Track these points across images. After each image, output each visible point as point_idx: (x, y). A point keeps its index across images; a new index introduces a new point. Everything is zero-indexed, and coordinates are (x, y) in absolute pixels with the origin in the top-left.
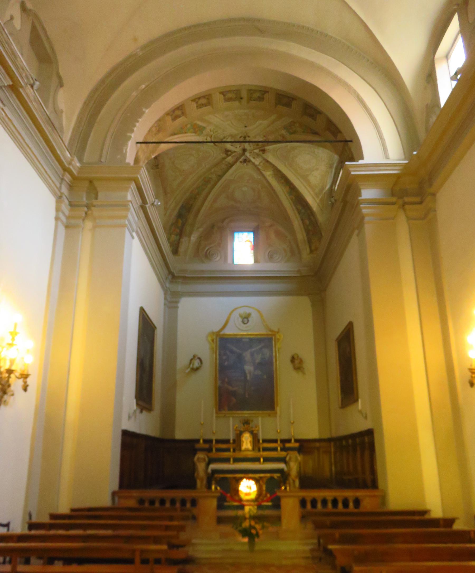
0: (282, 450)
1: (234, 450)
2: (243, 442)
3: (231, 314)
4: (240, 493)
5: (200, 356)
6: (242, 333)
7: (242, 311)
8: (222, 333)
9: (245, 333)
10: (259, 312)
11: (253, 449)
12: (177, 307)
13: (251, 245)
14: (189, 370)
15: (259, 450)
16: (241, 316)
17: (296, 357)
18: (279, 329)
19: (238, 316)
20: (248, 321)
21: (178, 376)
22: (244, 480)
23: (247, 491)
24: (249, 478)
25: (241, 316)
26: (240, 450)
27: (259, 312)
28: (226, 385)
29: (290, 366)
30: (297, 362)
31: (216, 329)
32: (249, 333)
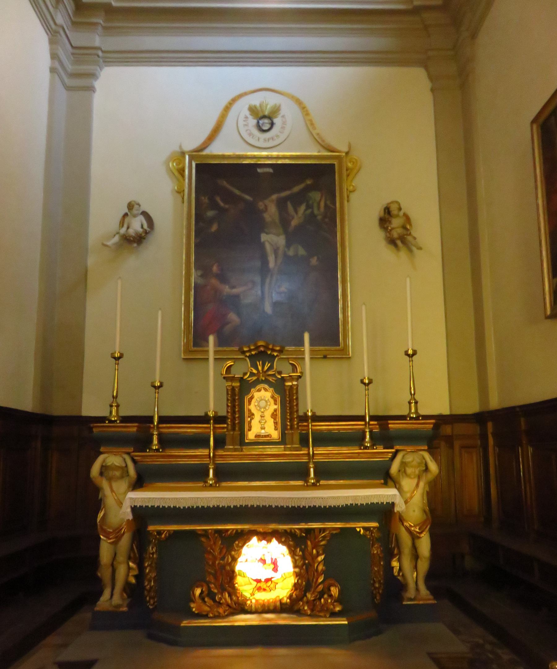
0: (376, 440)
1: (220, 443)
2: (252, 415)
3: (227, 109)
4: (239, 581)
5: (144, 208)
6: (256, 153)
7: (255, 100)
8: (205, 152)
9: (264, 153)
10: (299, 102)
11: (283, 440)
12: (91, 89)
13: (293, 582)
14: (116, 239)
15: (304, 442)
16: (253, 110)
17: (394, 208)
18: (350, 147)
19: (248, 113)
20: (272, 124)
21: (91, 261)
22: (255, 539)
23: (265, 572)
24: (265, 536)
25: (253, 110)
26: (242, 441)
27: (299, 102)
28: (214, 281)
29: (379, 235)
30: (396, 223)
31: (190, 145)
32: (275, 154)
